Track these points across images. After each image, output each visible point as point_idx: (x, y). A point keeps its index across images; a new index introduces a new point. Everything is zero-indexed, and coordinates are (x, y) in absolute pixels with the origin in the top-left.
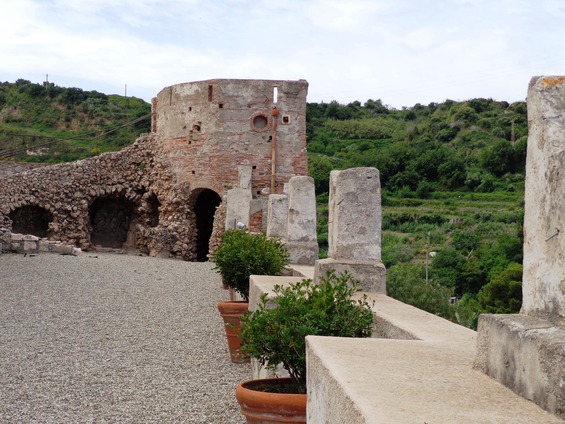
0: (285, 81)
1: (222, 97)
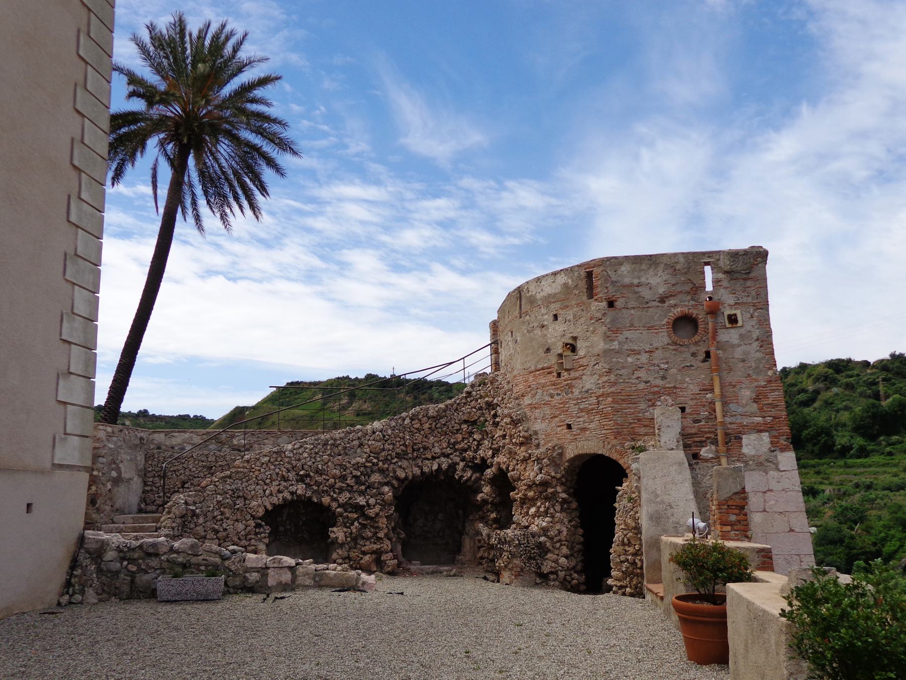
0: (723, 252)
1: (611, 289)
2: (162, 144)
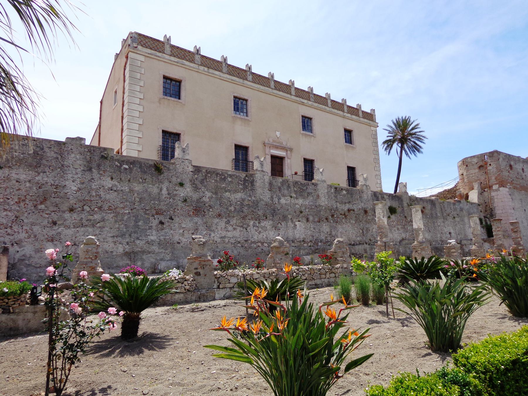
2: (397, 144)
